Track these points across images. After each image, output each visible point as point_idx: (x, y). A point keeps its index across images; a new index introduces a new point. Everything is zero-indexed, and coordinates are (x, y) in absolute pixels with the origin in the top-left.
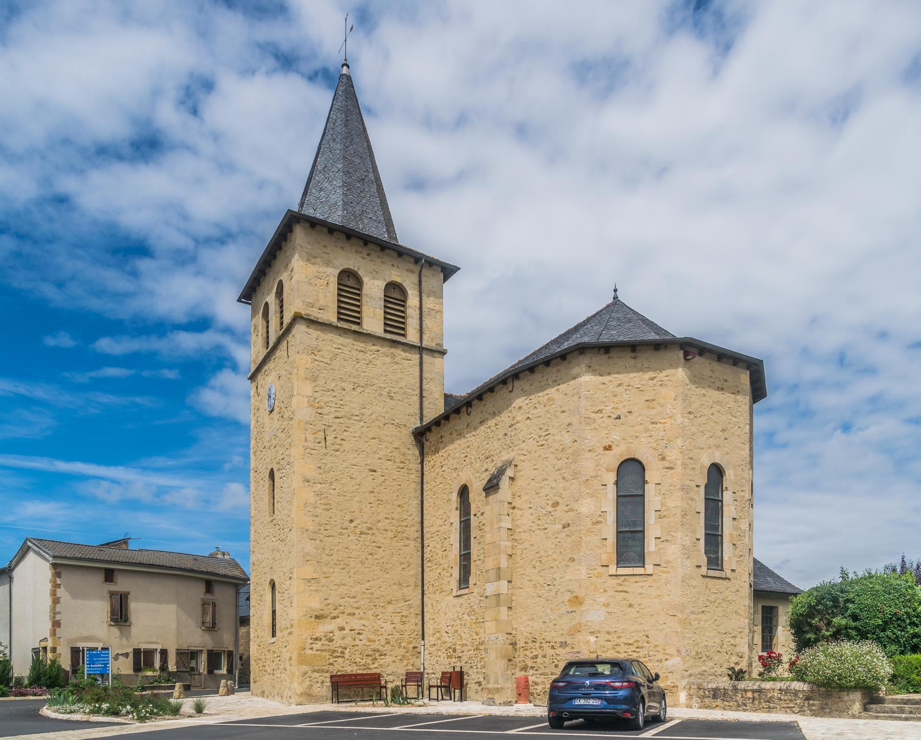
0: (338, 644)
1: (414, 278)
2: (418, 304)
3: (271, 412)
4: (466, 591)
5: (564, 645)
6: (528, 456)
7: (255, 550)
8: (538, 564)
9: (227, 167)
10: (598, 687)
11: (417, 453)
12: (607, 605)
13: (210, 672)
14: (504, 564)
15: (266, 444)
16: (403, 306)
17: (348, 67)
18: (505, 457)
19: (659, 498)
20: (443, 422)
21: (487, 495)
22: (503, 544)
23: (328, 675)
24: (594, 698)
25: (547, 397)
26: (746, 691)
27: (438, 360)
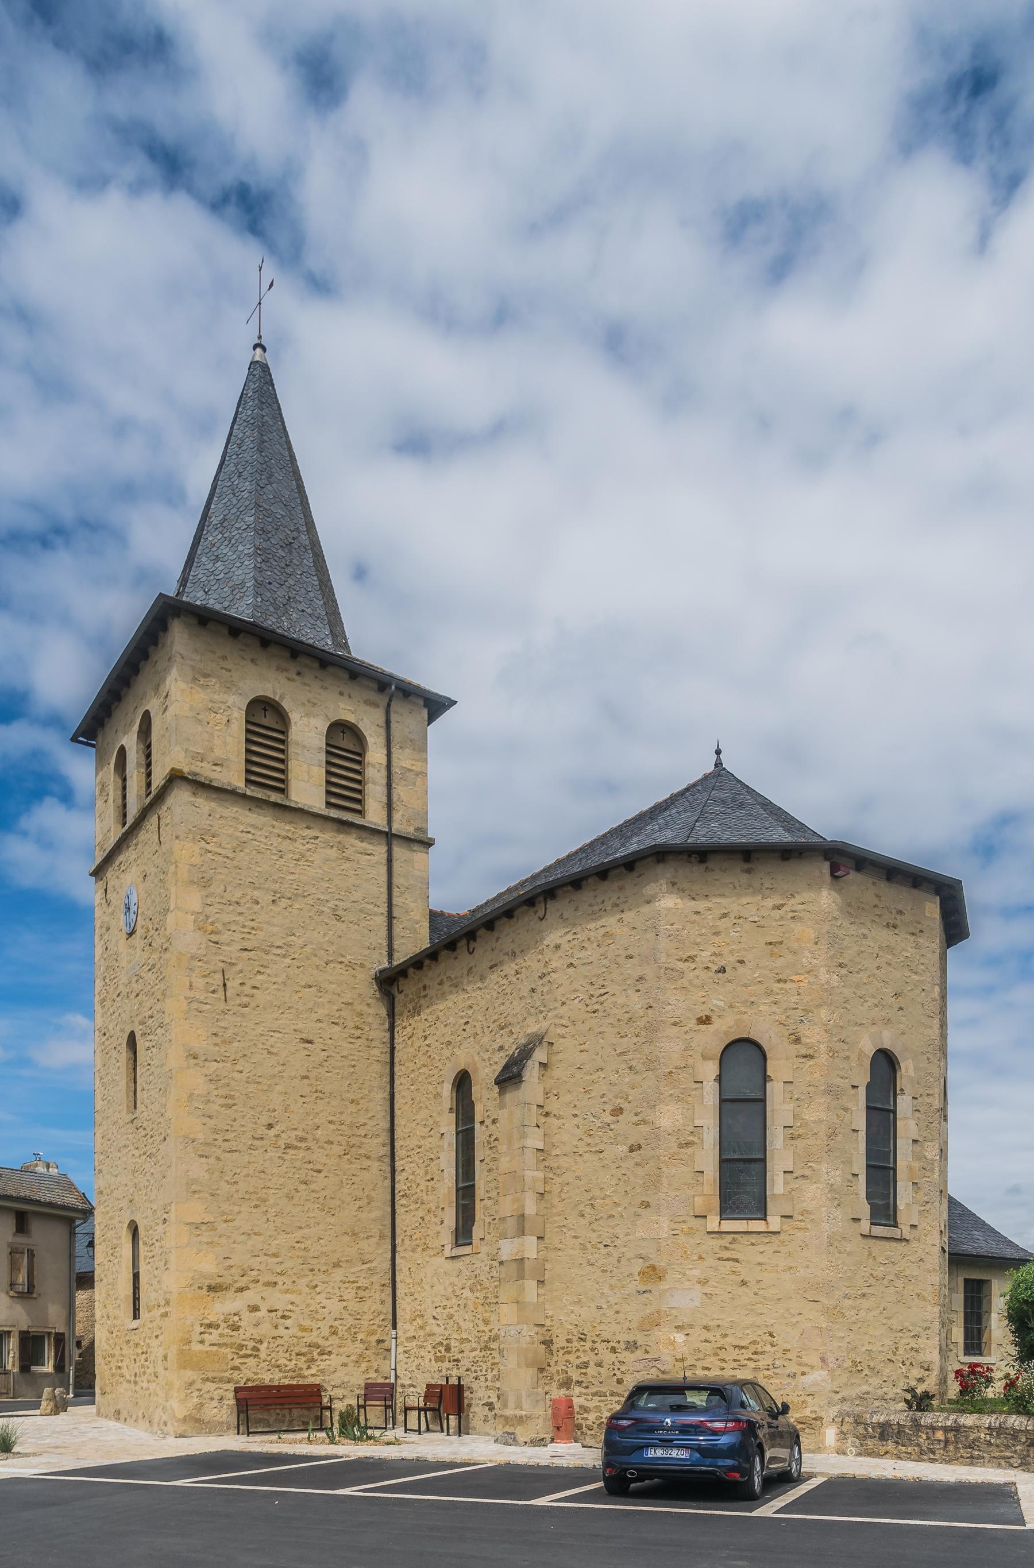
0: (248, 1335)
1: (379, 716)
2: (384, 761)
3: (131, 934)
4: (467, 1250)
5: (632, 1346)
6: (571, 1028)
7: (104, 1168)
8: (588, 1209)
9: (54, 387)
10: (686, 1429)
11: (383, 1012)
12: (704, 1282)
13: (25, 1369)
14: (530, 1208)
15: (121, 988)
16: (359, 763)
17: (264, 349)
18: (533, 1027)
19: (790, 1106)
20: (427, 962)
21: (502, 1092)
22: (529, 1174)
23: (231, 1387)
24: (678, 1447)
25: (602, 931)
26: (934, 1429)
27: (418, 856)
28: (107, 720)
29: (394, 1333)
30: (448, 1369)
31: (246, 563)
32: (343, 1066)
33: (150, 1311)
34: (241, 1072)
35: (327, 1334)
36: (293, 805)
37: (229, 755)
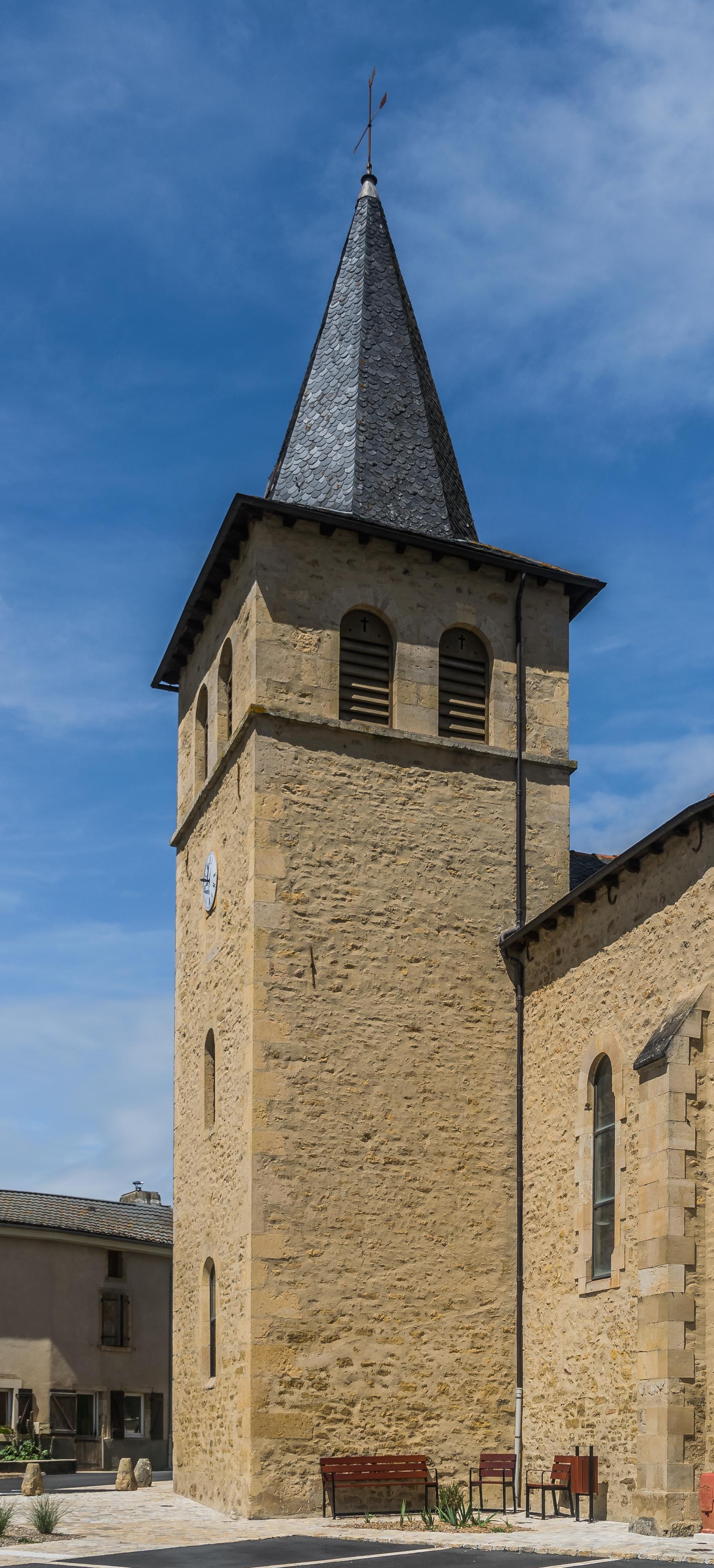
0: (337, 1395)
1: (506, 614)
3: (210, 912)
4: (604, 1284)
15: (201, 978)
17: (374, 180)
18: (687, 992)
20: (561, 919)
23: (316, 1458)
28: (189, 656)
29: (518, 1391)
30: (581, 1437)
31: (347, 444)
32: (458, 1058)
33: (225, 1367)
34: (332, 1071)
35: (435, 1393)
36: (397, 736)
37: (320, 682)
